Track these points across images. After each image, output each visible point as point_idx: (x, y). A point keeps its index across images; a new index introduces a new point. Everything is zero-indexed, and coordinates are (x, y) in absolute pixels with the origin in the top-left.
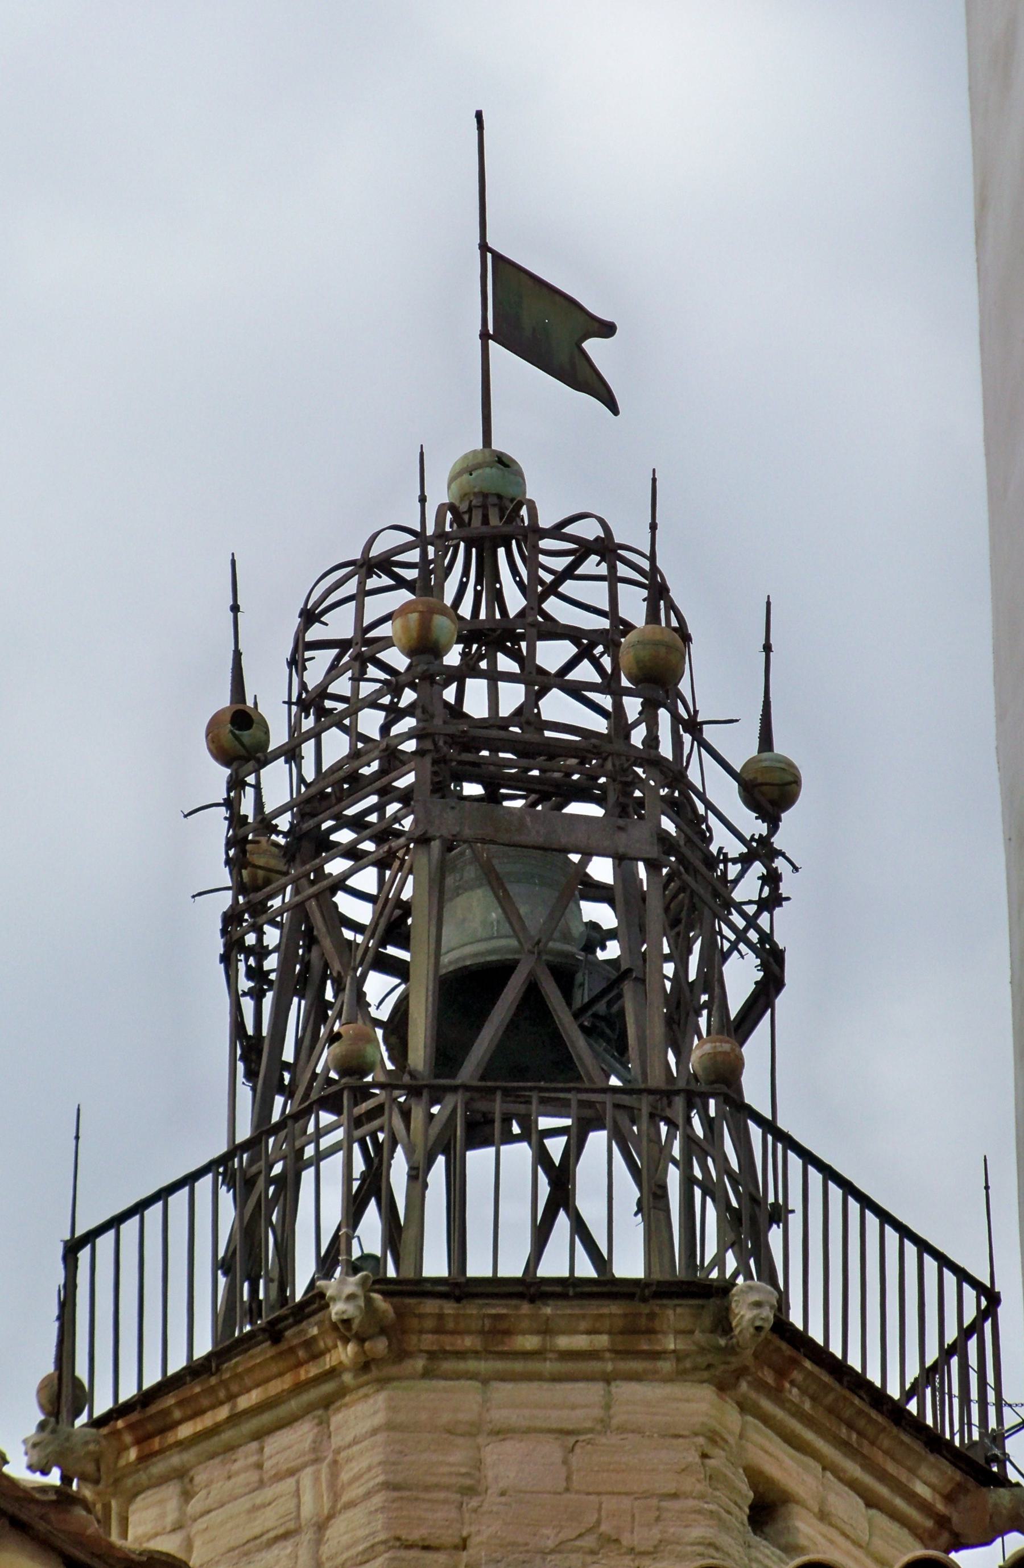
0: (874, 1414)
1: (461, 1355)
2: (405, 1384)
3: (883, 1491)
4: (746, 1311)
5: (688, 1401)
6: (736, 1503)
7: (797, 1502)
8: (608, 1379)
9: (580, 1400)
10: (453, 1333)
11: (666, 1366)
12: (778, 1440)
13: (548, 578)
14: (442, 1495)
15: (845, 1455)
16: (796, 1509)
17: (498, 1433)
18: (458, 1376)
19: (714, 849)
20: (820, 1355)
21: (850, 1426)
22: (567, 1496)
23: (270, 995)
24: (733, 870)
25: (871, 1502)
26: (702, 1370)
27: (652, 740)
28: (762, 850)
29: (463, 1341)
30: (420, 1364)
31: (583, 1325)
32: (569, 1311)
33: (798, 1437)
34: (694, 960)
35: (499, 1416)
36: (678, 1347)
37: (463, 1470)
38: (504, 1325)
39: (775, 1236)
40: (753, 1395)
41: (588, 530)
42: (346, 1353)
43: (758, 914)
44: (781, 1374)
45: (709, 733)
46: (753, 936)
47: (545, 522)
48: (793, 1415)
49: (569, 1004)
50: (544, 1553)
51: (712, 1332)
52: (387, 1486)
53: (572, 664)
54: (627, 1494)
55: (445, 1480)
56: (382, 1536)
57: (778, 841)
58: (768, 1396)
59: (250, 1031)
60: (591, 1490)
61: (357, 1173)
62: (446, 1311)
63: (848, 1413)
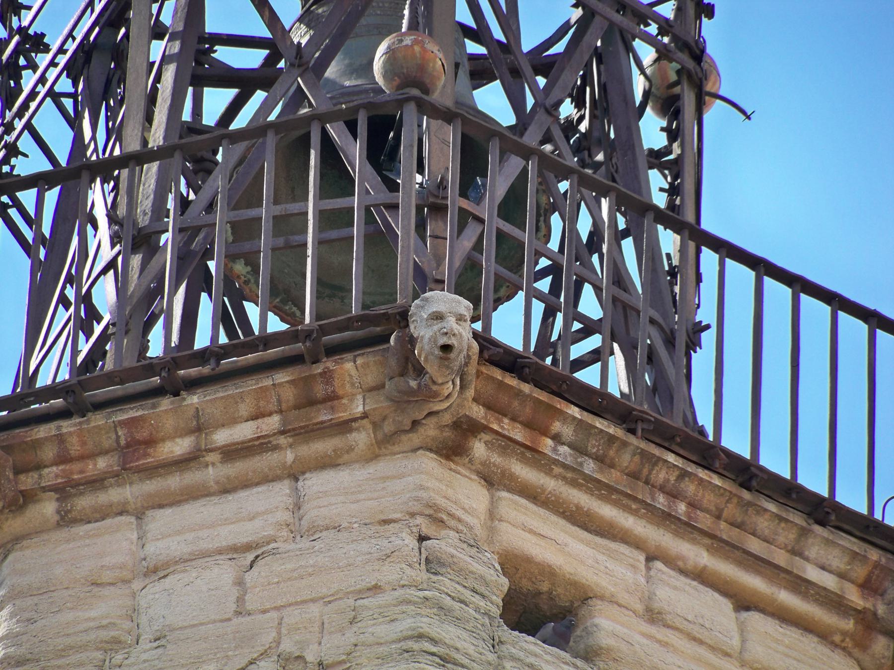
0: (702, 474)
1: (97, 483)
2: (45, 536)
5: (401, 476)
6: (474, 591)
7: (602, 598)
8: (294, 474)
9: (261, 509)
10: (82, 458)
11: (361, 438)
12: (562, 522)
15: (676, 534)
16: (598, 605)
17: (155, 571)
18: (102, 514)
21: (674, 495)
25: (744, 603)
26: (406, 432)
29: (95, 465)
30: (48, 508)
31: (244, 409)
32: (221, 395)
33: (589, 514)
35: (159, 548)
36: (367, 408)
38: (143, 434)
40: (496, 458)
48: (573, 483)
51: (402, 374)
54: (313, 601)
58: (523, 460)
60: (268, 606)
62: (64, 430)
63: (661, 475)
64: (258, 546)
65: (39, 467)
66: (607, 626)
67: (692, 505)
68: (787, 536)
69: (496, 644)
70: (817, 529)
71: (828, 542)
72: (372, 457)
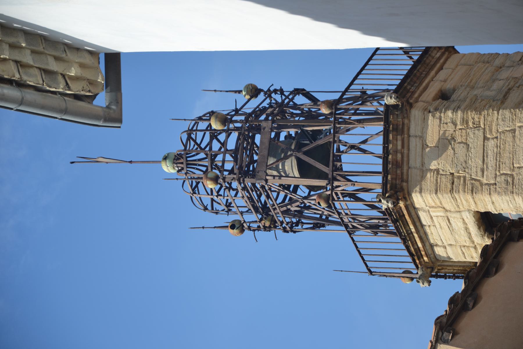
0: (418, 68)
1: (402, 173)
3: (438, 65)
4: (390, 101)
5: (415, 116)
8: (409, 136)
11: (406, 121)
12: (425, 92)
13: (196, 146)
14: (439, 179)
15: (429, 75)
18: (408, 175)
19: (267, 106)
20: (403, 81)
21: (422, 73)
22: (440, 147)
23: (302, 221)
24: (273, 101)
25: (441, 68)
27: (241, 122)
28: (269, 94)
30: (405, 184)
31: (395, 142)
34: (295, 112)
35: (418, 165)
37: (432, 174)
38: (395, 162)
39: (369, 92)
40: (413, 99)
41: (185, 137)
42: (402, 204)
43: (285, 95)
44: (408, 91)
45: (238, 107)
46: (290, 97)
47: (183, 148)
48: (418, 88)
49: (309, 144)
50: (455, 154)
52: (436, 193)
53: (219, 141)
55: (435, 178)
56: (450, 195)
57: (266, 90)
58: (414, 95)
59: (312, 226)
61: (349, 199)
64: (423, 144)
65: (396, 184)
66: (449, 86)
67: (424, 71)
68: (430, 58)
69: (454, 101)
70: (430, 53)
71: (432, 52)
72: (409, 121)
